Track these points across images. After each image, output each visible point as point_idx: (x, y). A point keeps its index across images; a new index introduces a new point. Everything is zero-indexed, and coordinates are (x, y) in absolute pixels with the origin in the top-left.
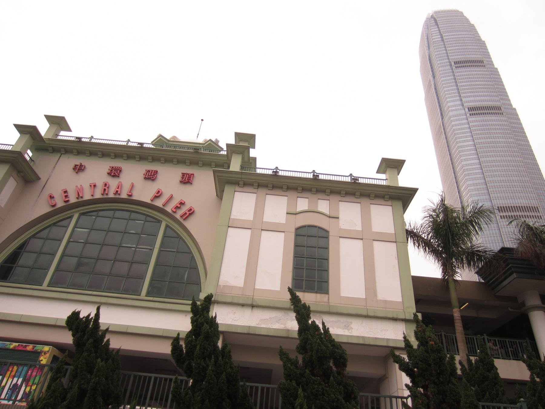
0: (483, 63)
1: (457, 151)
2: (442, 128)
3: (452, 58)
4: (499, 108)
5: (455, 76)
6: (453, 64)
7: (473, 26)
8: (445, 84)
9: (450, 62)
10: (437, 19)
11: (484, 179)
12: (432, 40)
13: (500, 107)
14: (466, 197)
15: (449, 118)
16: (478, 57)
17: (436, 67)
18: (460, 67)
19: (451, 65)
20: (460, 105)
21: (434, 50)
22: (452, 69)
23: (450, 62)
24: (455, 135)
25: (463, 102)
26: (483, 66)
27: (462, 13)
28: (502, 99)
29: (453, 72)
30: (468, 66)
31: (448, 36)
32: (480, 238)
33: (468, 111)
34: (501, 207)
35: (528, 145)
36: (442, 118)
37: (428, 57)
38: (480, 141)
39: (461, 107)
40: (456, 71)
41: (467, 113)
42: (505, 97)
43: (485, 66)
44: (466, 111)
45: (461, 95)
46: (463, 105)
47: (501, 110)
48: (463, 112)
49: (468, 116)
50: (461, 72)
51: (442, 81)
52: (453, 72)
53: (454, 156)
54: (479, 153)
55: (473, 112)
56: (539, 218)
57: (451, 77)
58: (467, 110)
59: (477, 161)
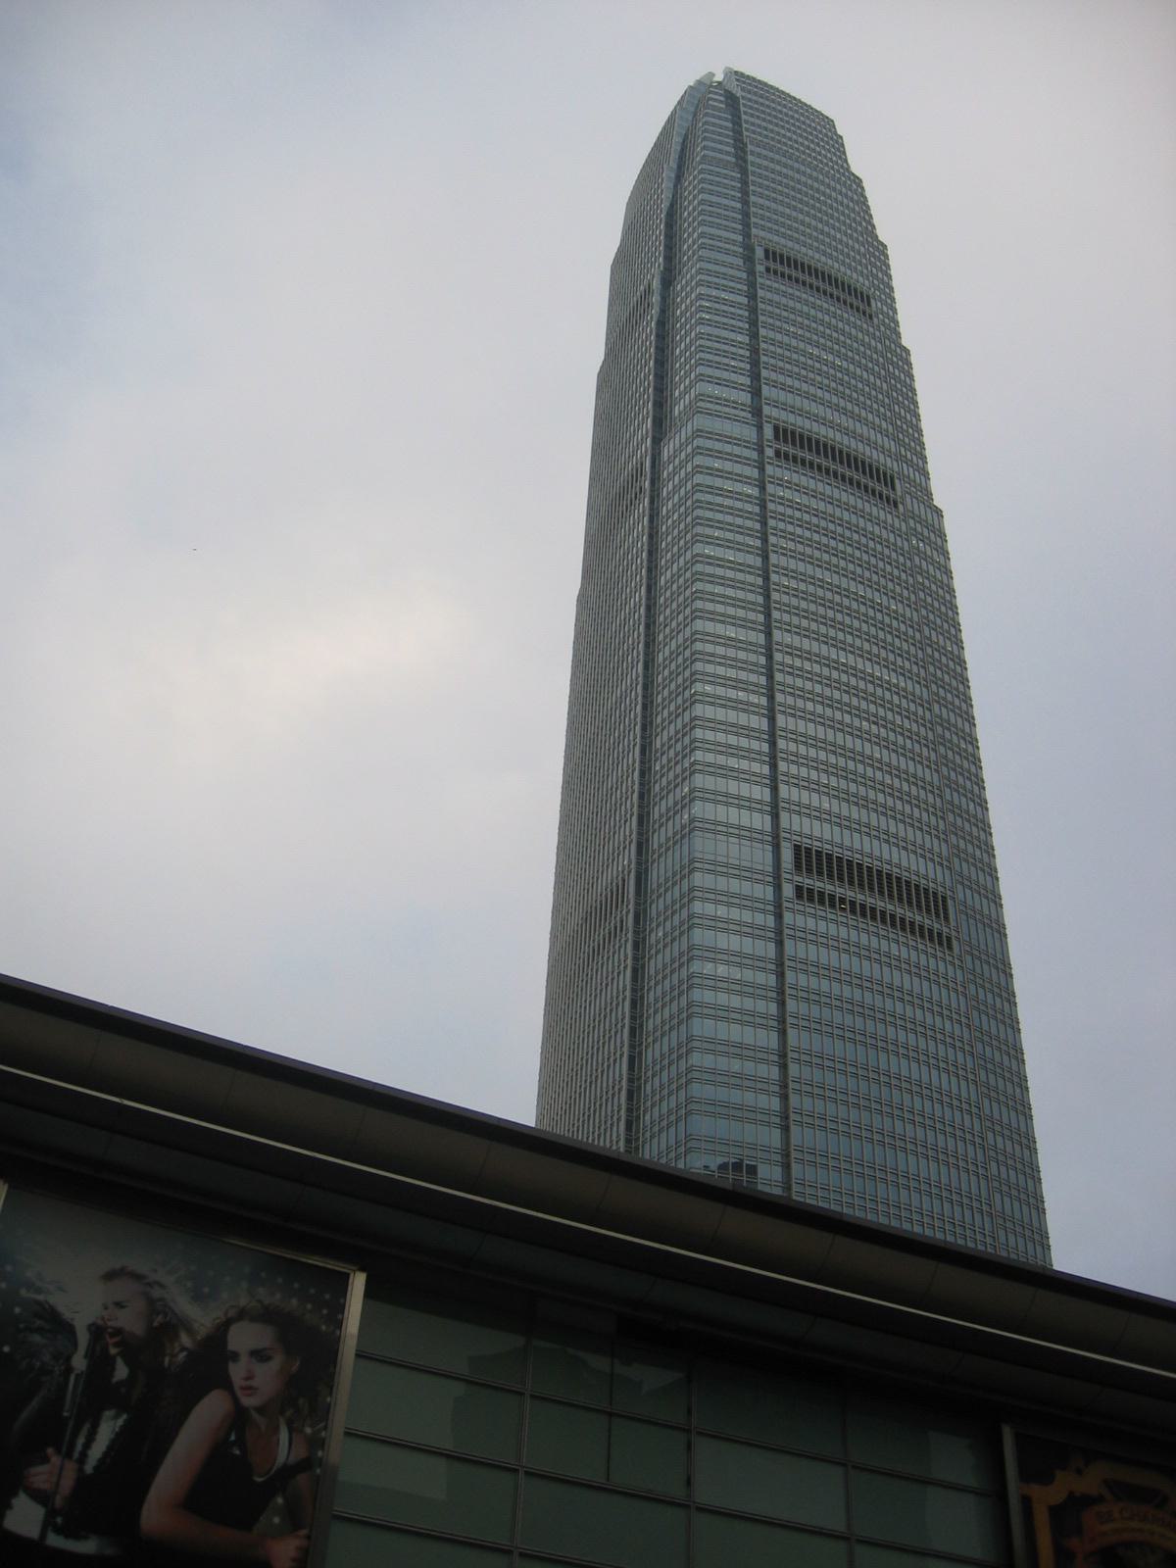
0: (869, 304)
2: (631, 907)
3: (775, 412)
4: (934, 902)
6: (759, 253)
7: (882, 249)
8: (708, 310)
9: (749, 249)
10: (750, 147)
11: (763, 557)
12: (702, 149)
13: (944, 899)
16: (862, 283)
17: (689, 243)
18: (783, 275)
19: (749, 259)
21: (700, 214)
22: (752, 273)
23: (749, 249)
24: (695, 523)
28: (943, 703)
29: (752, 285)
30: (827, 472)
31: (798, 488)
34: (810, 853)
35: (986, 844)
36: (657, 441)
37: (665, 206)
38: (761, 201)
40: (800, 921)
43: (896, 505)
46: (757, 412)
48: (750, 433)
49: (768, 440)
50: (793, 485)
51: (700, 297)
52: (752, 285)
56: (843, 290)
58: (768, 432)
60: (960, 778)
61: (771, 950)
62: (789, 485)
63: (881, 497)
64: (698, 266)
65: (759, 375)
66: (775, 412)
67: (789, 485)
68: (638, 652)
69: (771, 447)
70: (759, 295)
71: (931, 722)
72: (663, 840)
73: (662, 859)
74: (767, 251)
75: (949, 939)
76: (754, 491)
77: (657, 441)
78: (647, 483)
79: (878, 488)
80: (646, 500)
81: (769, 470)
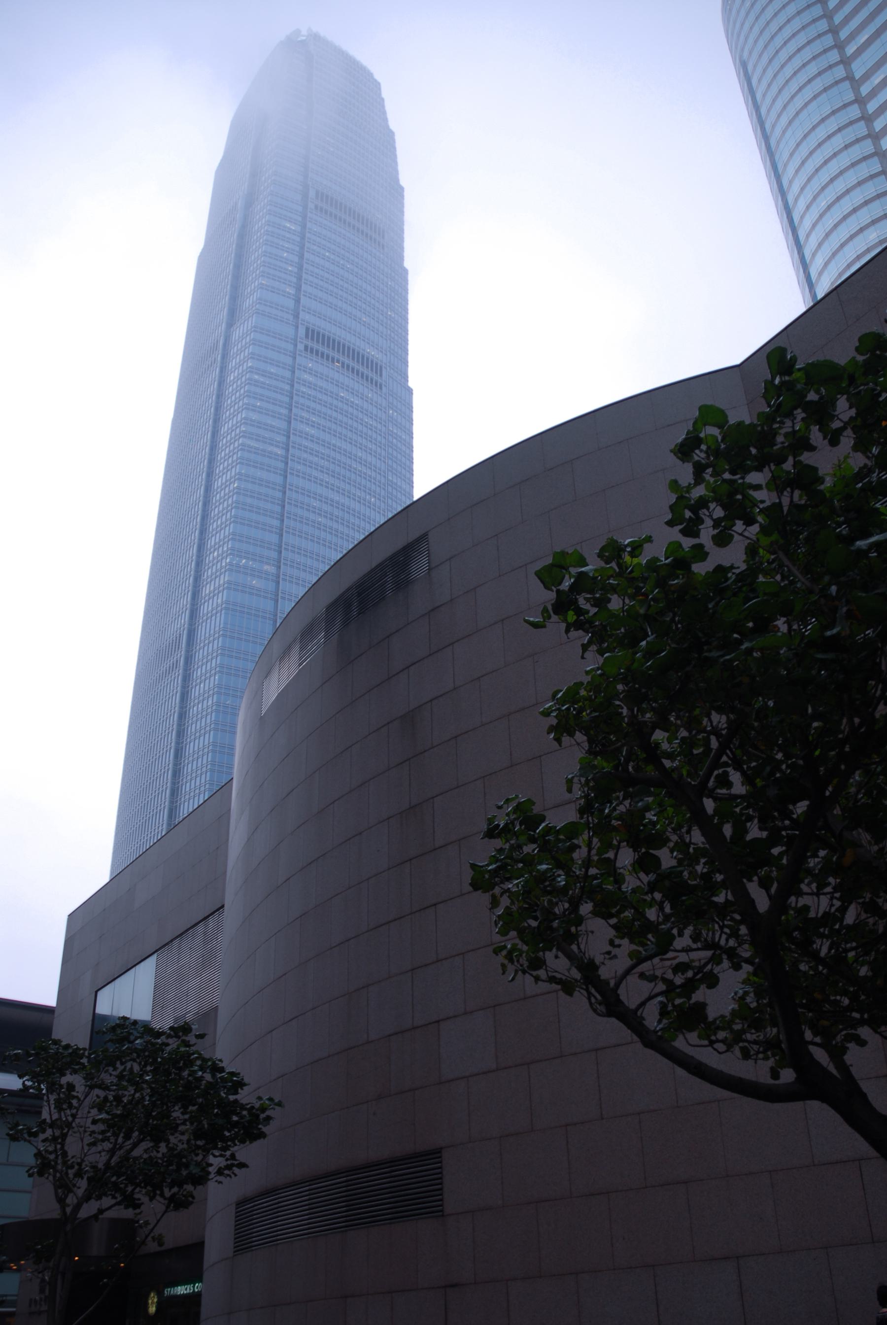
0: (383, 237)
1: (242, 391)
3: (307, 317)
4: (378, 369)
5: (300, 290)
13: (381, 367)
14: (214, 567)
15: (243, 334)
20: (292, 284)
25: (301, 308)
26: (379, 245)
27: (378, 85)
30: (340, 220)
32: (213, 694)
33: (304, 336)
36: (230, 325)
39: (291, 318)
41: (299, 340)
42: (404, 448)
44: (299, 335)
45: (306, 243)
46: (296, 316)
47: (381, 375)
48: (290, 331)
53: (228, 413)
54: (293, 447)
55: (315, 346)
56: (367, 226)
57: (275, 423)
58: (302, 331)
59: (283, 425)
60: (399, 494)
61: (271, 586)
62: (310, 372)
63: (371, 239)
64: (248, 376)
65: (303, 255)
66: (307, 317)
67: (310, 372)
68: (196, 522)
69: (302, 343)
70: (304, 267)
71: (385, 445)
72: (219, 484)
73: (208, 585)
74: (317, 192)
75: (381, 385)
76: (289, 360)
77: (231, 324)
78: (219, 356)
79: (370, 375)
80: (218, 369)
81: (299, 360)
